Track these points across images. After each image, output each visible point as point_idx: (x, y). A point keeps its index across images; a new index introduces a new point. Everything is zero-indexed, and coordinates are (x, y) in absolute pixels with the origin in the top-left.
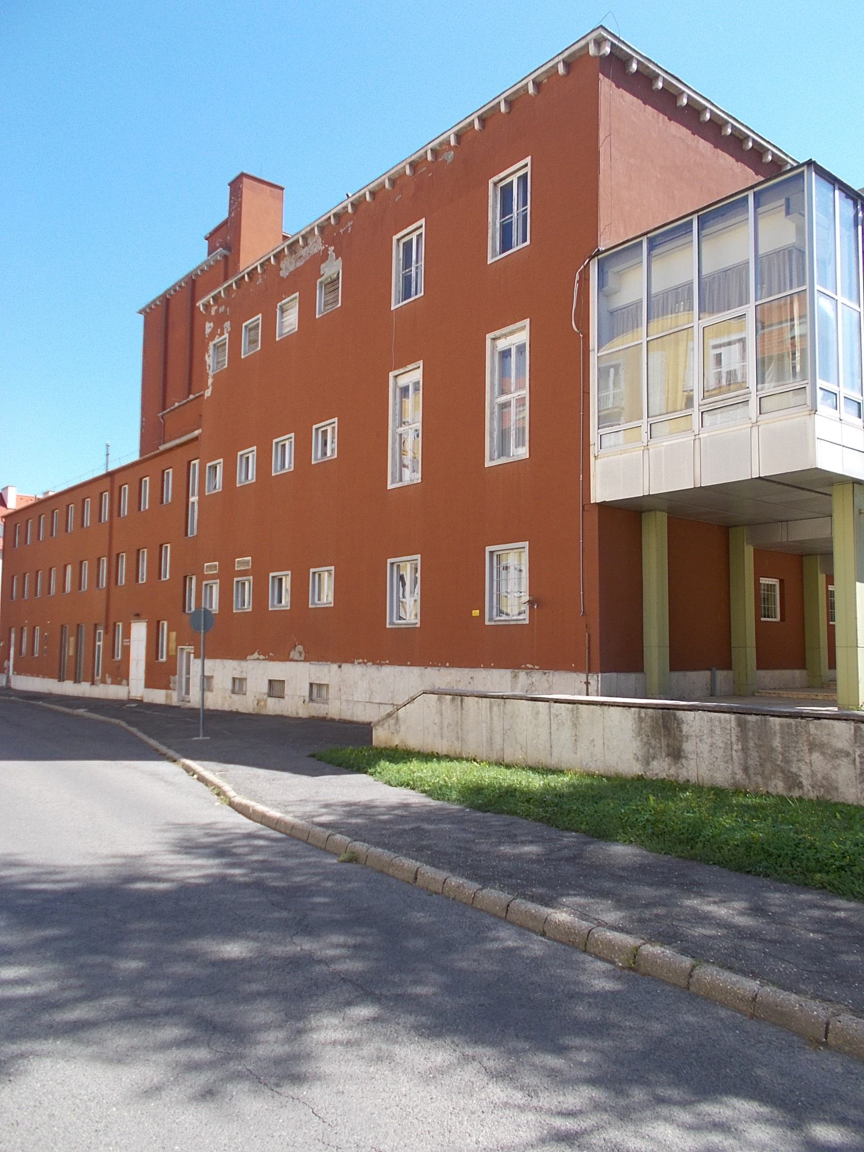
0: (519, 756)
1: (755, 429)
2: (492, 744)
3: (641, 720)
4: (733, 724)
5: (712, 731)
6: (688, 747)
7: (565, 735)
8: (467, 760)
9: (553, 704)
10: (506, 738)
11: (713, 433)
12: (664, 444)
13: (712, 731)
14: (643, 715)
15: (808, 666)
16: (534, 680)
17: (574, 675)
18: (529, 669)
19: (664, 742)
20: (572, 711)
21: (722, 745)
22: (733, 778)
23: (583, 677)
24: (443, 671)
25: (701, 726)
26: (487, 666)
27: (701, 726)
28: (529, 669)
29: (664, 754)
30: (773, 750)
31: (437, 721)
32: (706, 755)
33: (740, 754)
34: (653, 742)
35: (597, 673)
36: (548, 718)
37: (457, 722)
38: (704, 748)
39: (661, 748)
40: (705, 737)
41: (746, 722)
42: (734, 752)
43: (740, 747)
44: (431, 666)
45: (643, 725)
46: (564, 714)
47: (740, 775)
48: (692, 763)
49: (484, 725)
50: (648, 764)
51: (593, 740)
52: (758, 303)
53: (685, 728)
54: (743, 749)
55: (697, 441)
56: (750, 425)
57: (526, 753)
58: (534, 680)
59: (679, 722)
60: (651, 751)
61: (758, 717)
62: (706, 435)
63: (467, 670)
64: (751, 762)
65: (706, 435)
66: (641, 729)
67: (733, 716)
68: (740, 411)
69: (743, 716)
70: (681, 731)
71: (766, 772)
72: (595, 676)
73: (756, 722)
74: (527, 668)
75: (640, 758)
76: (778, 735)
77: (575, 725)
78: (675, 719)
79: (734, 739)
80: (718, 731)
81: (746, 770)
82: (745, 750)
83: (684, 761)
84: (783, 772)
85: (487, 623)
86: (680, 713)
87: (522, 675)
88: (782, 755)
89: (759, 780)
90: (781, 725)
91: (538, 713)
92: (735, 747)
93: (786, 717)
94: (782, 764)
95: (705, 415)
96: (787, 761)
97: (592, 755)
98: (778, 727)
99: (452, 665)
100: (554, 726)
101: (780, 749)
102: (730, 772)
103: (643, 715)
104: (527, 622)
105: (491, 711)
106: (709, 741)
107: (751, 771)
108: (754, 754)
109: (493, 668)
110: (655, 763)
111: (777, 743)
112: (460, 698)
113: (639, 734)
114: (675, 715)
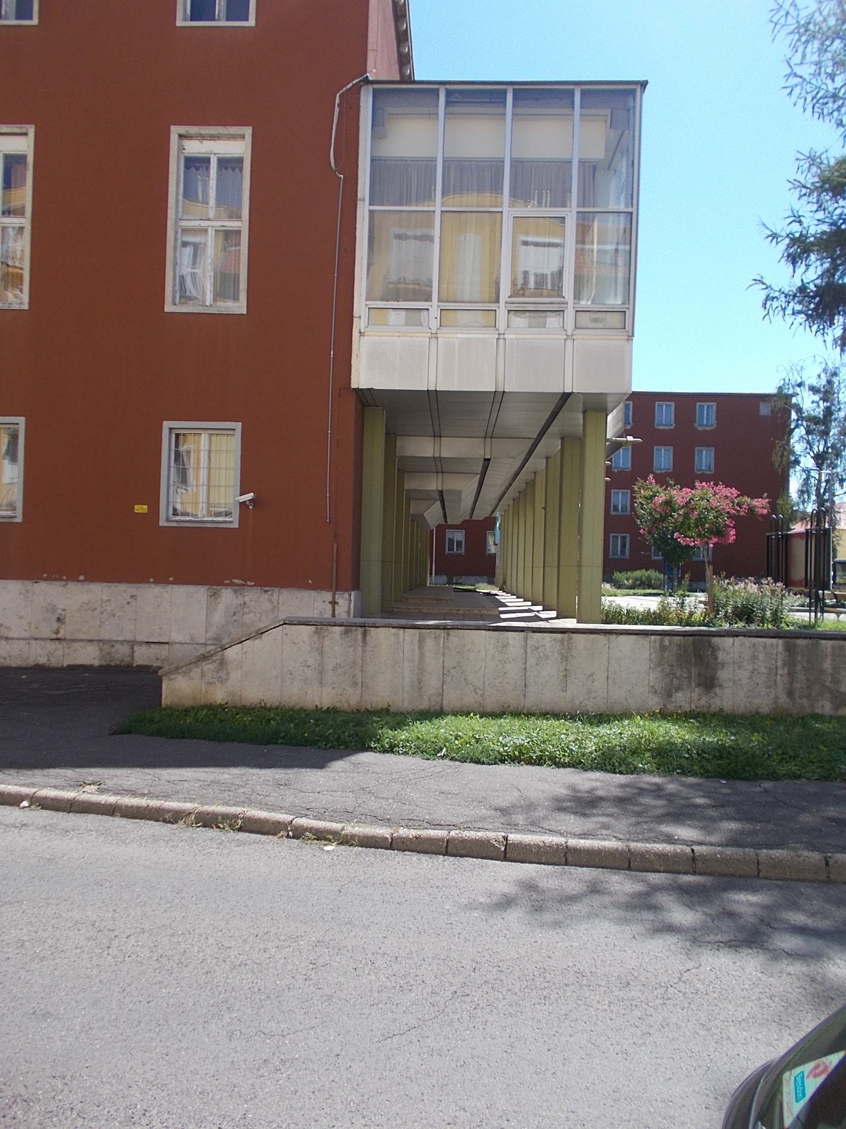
0: (471, 699)
1: (569, 342)
2: (420, 688)
3: (663, 648)
4: (780, 649)
5: (754, 657)
6: (723, 675)
7: (550, 670)
8: (455, 714)
9: (530, 634)
10: (448, 679)
11: (522, 336)
12: (459, 336)
13: (754, 657)
14: (667, 643)
15: (361, 586)
16: (246, 599)
17: (313, 593)
18: (236, 585)
19: (694, 671)
20: (562, 641)
21: (764, 671)
22: (775, 703)
23: (328, 596)
24: (72, 586)
25: (741, 652)
26: (162, 580)
27: (741, 652)
28: (236, 585)
29: (693, 685)
30: (822, 671)
31: (311, 662)
32: (745, 681)
33: (785, 678)
34: (678, 672)
35: (347, 590)
36: (522, 651)
37: (354, 662)
38: (743, 675)
39: (690, 677)
40: (745, 663)
41: (795, 645)
42: (778, 676)
43: (786, 671)
44: (45, 580)
45: (666, 654)
46: (548, 645)
47: (783, 699)
48: (728, 691)
49: (407, 664)
50: (669, 695)
51: (592, 675)
52: (444, 209)
53: (721, 656)
54: (789, 673)
55: (501, 341)
56: (565, 337)
57: (482, 696)
58: (246, 599)
59: (714, 650)
60: (675, 682)
61: (808, 641)
62: (513, 336)
63: (123, 587)
64: (797, 685)
65: (513, 336)
66: (662, 658)
67: (781, 641)
68: (553, 321)
69: (792, 640)
70: (716, 659)
71: (813, 694)
72: (346, 595)
73: (807, 646)
74: (232, 584)
75: (659, 691)
76: (829, 658)
77: (565, 659)
78: (710, 646)
79: (779, 664)
80: (761, 657)
81: (790, 693)
82: (791, 674)
83: (717, 690)
84: (831, 691)
85: (163, 523)
86: (716, 640)
87: (227, 596)
88: (832, 676)
89: (805, 702)
90: (833, 648)
91: (505, 646)
92: (780, 672)
93: (839, 639)
94: (831, 685)
95: (619, 315)
96: (836, 681)
97: (589, 691)
98: (829, 650)
99: (92, 578)
100: (531, 661)
101: (830, 671)
102: (772, 696)
103: (667, 643)
104: (236, 525)
105: (421, 646)
106: (750, 667)
107: (797, 695)
108: (801, 677)
109: (172, 583)
110: (679, 694)
111: (827, 665)
112: (360, 630)
113: (660, 664)
114: (710, 642)
